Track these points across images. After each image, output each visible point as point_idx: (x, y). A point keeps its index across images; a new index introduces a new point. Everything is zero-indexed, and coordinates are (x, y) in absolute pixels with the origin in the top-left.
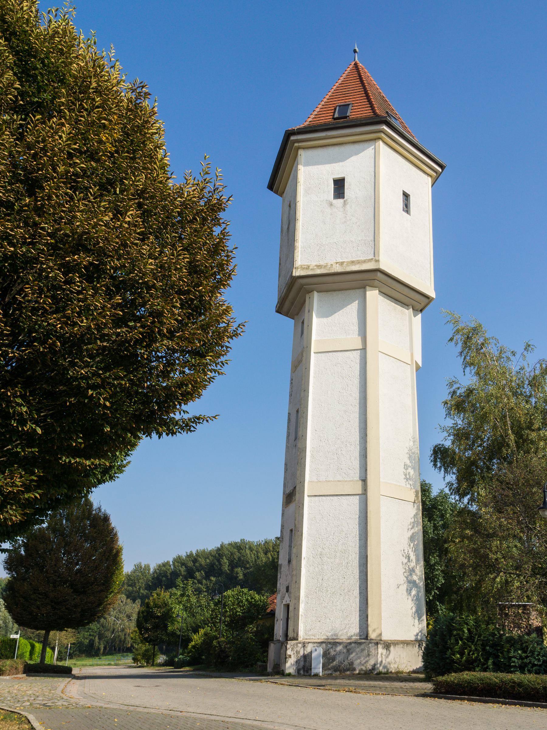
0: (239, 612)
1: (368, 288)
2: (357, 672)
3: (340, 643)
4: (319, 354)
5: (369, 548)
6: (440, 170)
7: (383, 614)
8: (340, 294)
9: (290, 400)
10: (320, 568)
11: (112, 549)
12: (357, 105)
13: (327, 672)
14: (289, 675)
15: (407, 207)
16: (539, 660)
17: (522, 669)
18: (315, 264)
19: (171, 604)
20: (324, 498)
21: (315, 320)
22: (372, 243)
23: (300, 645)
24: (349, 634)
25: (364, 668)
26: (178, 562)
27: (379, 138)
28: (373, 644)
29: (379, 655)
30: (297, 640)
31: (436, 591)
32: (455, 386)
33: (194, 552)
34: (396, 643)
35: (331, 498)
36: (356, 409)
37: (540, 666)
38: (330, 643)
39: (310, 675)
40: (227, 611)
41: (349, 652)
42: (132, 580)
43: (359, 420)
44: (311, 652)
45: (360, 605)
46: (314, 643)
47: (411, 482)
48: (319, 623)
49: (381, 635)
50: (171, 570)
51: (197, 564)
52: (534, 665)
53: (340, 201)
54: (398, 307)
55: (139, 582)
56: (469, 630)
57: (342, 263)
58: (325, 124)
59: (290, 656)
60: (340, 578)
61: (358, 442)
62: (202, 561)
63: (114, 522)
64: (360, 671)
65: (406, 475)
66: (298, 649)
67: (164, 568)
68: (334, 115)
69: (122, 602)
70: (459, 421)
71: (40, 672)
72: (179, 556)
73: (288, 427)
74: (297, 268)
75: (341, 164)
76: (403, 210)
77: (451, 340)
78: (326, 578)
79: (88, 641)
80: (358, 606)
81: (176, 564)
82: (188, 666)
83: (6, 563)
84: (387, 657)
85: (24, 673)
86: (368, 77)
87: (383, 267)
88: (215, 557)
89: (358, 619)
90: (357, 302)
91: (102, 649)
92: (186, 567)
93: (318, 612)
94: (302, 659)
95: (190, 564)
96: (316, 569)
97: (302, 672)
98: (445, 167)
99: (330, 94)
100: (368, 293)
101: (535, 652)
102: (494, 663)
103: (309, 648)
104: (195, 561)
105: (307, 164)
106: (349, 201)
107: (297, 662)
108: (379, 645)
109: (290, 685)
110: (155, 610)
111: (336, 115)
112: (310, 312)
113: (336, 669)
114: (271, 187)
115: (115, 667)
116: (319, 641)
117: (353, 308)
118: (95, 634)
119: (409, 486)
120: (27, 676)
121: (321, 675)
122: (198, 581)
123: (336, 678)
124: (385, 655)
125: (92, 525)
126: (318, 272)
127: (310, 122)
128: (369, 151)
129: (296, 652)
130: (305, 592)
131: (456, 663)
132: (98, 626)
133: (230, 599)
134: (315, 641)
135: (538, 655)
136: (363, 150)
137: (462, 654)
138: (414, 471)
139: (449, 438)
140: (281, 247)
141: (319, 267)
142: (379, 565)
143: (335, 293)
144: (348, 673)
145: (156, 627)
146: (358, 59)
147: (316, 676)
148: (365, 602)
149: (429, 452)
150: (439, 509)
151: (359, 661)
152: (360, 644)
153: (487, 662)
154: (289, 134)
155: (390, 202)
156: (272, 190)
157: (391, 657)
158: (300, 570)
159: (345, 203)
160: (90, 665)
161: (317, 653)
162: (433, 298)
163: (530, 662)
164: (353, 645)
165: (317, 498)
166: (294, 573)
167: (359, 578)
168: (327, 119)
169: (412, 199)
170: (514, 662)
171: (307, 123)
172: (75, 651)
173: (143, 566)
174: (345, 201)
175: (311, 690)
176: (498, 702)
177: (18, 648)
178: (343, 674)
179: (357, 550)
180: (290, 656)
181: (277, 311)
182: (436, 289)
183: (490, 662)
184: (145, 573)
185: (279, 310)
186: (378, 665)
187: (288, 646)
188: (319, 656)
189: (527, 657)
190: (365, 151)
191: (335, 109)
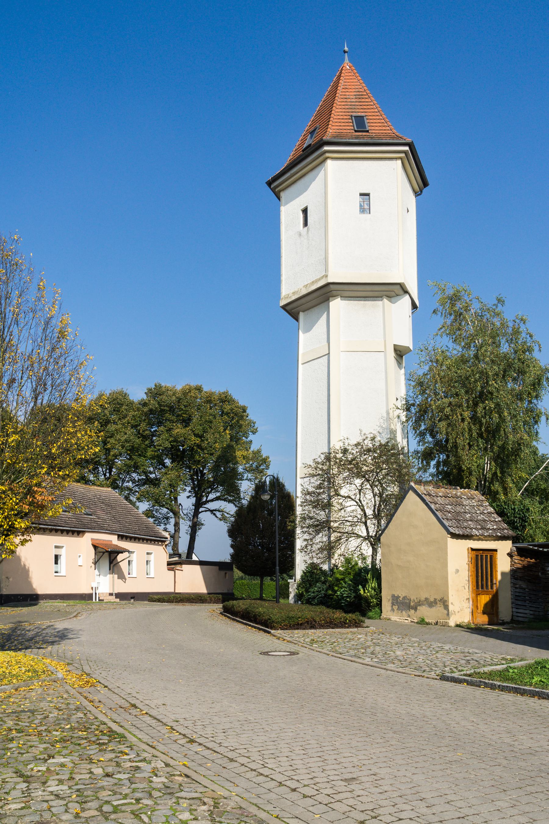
8: (316, 310)
18: (292, 292)
22: (324, 261)
126: (294, 298)
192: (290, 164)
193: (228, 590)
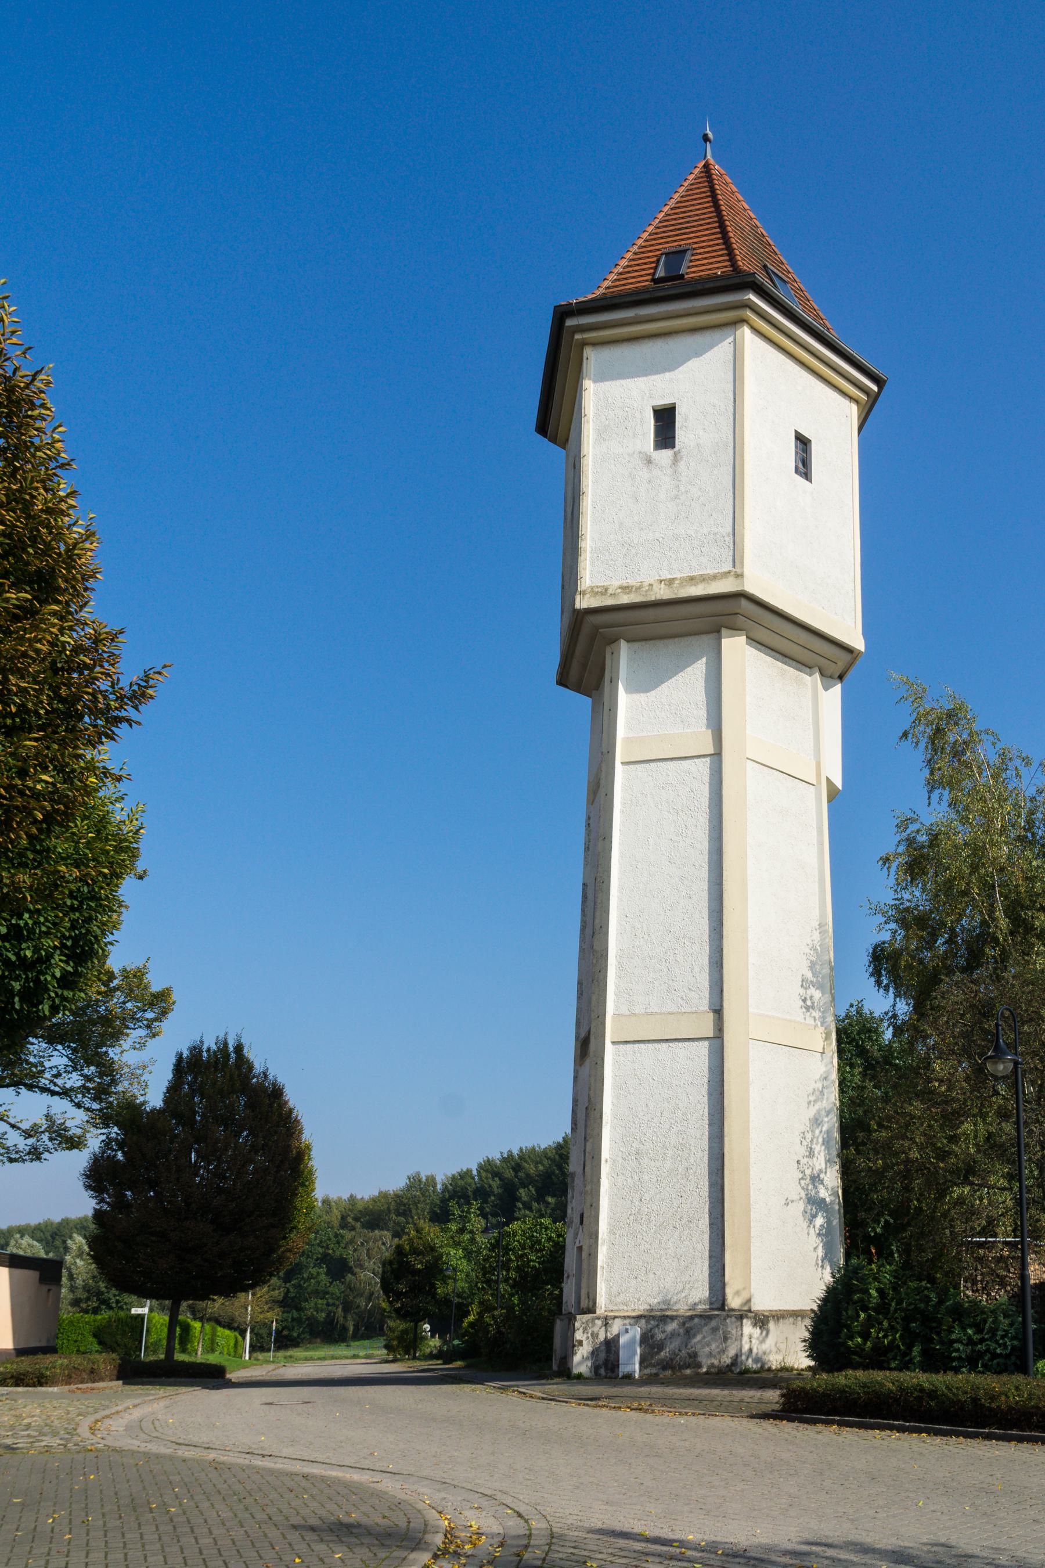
0: (533, 1261)
1: (724, 631)
2: (704, 1370)
3: (672, 1318)
4: (632, 766)
5: (726, 1139)
6: (875, 388)
7: (754, 1263)
8: (672, 647)
9: (585, 858)
10: (637, 1178)
11: (287, 1148)
12: (702, 250)
13: (647, 1371)
14: (579, 1377)
15: (804, 467)
16: (1005, 1346)
17: (972, 1362)
18: (617, 583)
19: (441, 1247)
20: (642, 1046)
21: (623, 698)
22: (729, 539)
23: (599, 1322)
24: (690, 1301)
25: (716, 1362)
26: (487, 1171)
27: (743, 321)
28: (733, 1319)
29: (745, 1339)
30: (595, 1312)
31: (888, 1218)
32: (913, 827)
33: (515, 1152)
34: (779, 1316)
35: (656, 1045)
36: (704, 873)
37: (1007, 1356)
38: (654, 1317)
39: (616, 1377)
40: (510, 1260)
41: (689, 1333)
42: (404, 1205)
43: (709, 894)
44: (618, 1336)
45: (710, 1246)
46: (625, 1317)
47: (816, 1014)
48: (634, 1281)
49: (749, 1301)
50: (474, 1186)
51: (521, 1174)
52: (994, 1356)
53: (667, 453)
54: (791, 671)
55: (417, 1208)
56: (880, 1291)
57: (670, 582)
58: (637, 292)
59: (581, 1343)
60: (674, 1196)
61: (706, 938)
62: (531, 1169)
63: (295, 1098)
64: (709, 1367)
65: (804, 1000)
66: (596, 1329)
67: (461, 1183)
68: (654, 274)
69: (384, 1244)
70: (916, 897)
71: (160, 1376)
72: (488, 1160)
73: (583, 911)
74: (583, 593)
75: (668, 375)
76: (797, 471)
77: (905, 735)
78: (647, 1196)
79: (324, 1315)
80: (707, 1248)
81: (484, 1174)
82: (462, 1359)
83: (87, 1177)
84: (763, 1341)
85: (118, 1379)
86: (733, 193)
87: (750, 588)
88: (553, 1160)
89: (706, 1273)
90: (704, 660)
91: (351, 1328)
92: (500, 1179)
93: (633, 1265)
94: (603, 1348)
95: (509, 1174)
96: (629, 1180)
97: (602, 1371)
98: (885, 381)
99: (650, 229)
100: (725, 642)
101: (997, 1330)
102: (924, 1353)
103: (616, 1328)
104: (517, 1168)
105: (600, 378)
106: (684, 452)
107: (593, 1353)
108: (745, 1321)
109: (543, 1399)
110: (411, 1259)
111: (661, 273)
112: (614, 681)
113: (666, 1365)
114: (543, 427)
115: (363, 1361)
116: (634, 1314)
117: (697, 671)
118: (337, 1303)
119: (812, 1022)
120: (124, 1384)
121: (637, 1376)
122: (524, 1203)
123: (663, 1383)
124: (758, 1339)
125: (250, 1106)
126: (625, 599)
127: (608, 288)
128: (722, 350)
129: (592, 1334)
130: (609, 1224)
131: (855, 1353)
132: (342, 1287)
133: (517, 1238)
134: (626, 1314)
135: (1003, 1337)
136: (711, 347)
137: (866, 1336)
138: (823, 994)
139: (887, 927)
140: (564, 554)
141: (626, 589)
142: (747, 1170)
143: (660, 644)
144: (688, 1372)
145: (415, 1290)
146: (713, 156)
147: (628, 1377)
148: (720, 1241)
149: (864, 959)
150: (896, 1065)
151: (707, 1349)
152: (710, 1318)
153: (911, 1351)
154: (562, 314)
155: (768, 454)
156: (545, 436)
157: (770, 1343)
158: (599, 1182)
159: (676, 459)
160: (319, 1359)
161: (630, 1336)
162: (860, 652)
163: (988, 1350)
164: (696, 1320)
165: (629, 1046)
166: (588, 1188)
167: (710, 1197)
168: (643, 281)
169: (814, 448)
170: (958, 1350)
171: (602, 291)
172: (303, 1332)
173: (424, 1179)
174: (675, 454)
175: (575, 1409)
176: (891, 1428)
177: (147, 1331)
178: (678, 1374)
179: (705, 1143)
180: (581, 1343)
181: (560, 683)
182: (866, 633)
183: (916, 1350)
184: (428, 1190)
185: (563, 681)
186: (744, 1357)
187: (577, 1325)
188: (632, 1342)
189: (982, 1341)
190: (716, 349)
191: (658, 261)
192: (603, 297)
193: (48, 1341)
